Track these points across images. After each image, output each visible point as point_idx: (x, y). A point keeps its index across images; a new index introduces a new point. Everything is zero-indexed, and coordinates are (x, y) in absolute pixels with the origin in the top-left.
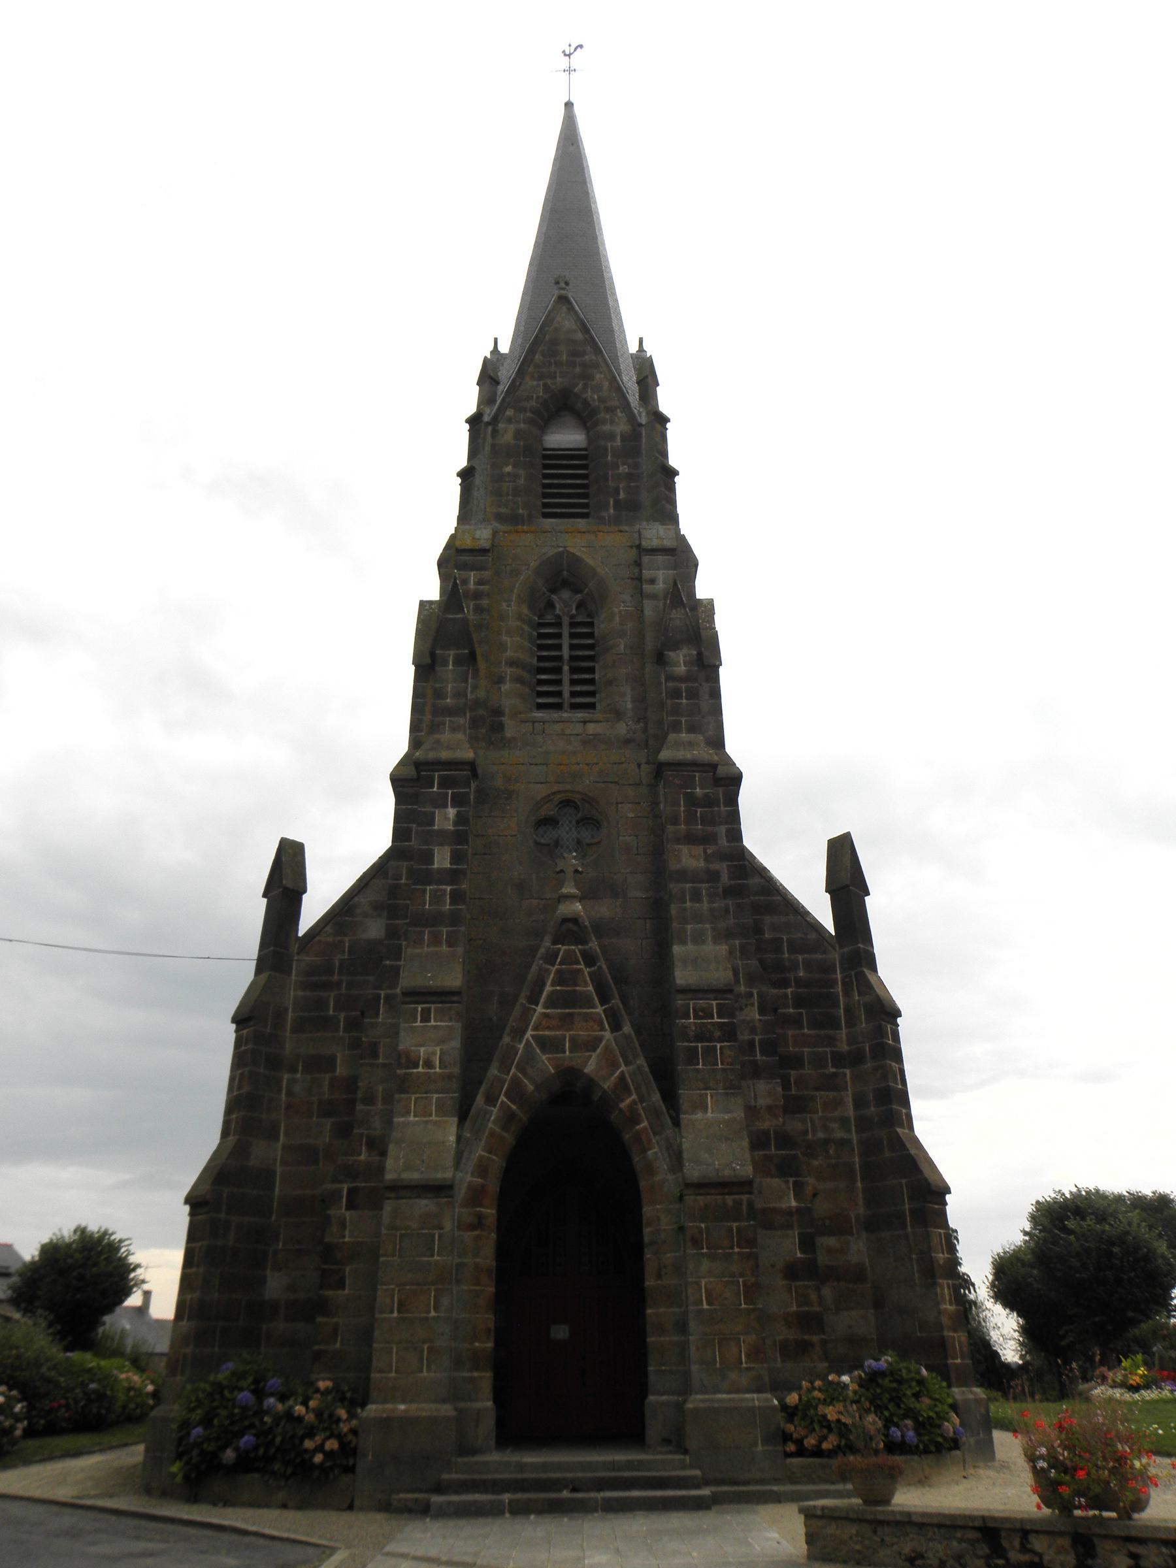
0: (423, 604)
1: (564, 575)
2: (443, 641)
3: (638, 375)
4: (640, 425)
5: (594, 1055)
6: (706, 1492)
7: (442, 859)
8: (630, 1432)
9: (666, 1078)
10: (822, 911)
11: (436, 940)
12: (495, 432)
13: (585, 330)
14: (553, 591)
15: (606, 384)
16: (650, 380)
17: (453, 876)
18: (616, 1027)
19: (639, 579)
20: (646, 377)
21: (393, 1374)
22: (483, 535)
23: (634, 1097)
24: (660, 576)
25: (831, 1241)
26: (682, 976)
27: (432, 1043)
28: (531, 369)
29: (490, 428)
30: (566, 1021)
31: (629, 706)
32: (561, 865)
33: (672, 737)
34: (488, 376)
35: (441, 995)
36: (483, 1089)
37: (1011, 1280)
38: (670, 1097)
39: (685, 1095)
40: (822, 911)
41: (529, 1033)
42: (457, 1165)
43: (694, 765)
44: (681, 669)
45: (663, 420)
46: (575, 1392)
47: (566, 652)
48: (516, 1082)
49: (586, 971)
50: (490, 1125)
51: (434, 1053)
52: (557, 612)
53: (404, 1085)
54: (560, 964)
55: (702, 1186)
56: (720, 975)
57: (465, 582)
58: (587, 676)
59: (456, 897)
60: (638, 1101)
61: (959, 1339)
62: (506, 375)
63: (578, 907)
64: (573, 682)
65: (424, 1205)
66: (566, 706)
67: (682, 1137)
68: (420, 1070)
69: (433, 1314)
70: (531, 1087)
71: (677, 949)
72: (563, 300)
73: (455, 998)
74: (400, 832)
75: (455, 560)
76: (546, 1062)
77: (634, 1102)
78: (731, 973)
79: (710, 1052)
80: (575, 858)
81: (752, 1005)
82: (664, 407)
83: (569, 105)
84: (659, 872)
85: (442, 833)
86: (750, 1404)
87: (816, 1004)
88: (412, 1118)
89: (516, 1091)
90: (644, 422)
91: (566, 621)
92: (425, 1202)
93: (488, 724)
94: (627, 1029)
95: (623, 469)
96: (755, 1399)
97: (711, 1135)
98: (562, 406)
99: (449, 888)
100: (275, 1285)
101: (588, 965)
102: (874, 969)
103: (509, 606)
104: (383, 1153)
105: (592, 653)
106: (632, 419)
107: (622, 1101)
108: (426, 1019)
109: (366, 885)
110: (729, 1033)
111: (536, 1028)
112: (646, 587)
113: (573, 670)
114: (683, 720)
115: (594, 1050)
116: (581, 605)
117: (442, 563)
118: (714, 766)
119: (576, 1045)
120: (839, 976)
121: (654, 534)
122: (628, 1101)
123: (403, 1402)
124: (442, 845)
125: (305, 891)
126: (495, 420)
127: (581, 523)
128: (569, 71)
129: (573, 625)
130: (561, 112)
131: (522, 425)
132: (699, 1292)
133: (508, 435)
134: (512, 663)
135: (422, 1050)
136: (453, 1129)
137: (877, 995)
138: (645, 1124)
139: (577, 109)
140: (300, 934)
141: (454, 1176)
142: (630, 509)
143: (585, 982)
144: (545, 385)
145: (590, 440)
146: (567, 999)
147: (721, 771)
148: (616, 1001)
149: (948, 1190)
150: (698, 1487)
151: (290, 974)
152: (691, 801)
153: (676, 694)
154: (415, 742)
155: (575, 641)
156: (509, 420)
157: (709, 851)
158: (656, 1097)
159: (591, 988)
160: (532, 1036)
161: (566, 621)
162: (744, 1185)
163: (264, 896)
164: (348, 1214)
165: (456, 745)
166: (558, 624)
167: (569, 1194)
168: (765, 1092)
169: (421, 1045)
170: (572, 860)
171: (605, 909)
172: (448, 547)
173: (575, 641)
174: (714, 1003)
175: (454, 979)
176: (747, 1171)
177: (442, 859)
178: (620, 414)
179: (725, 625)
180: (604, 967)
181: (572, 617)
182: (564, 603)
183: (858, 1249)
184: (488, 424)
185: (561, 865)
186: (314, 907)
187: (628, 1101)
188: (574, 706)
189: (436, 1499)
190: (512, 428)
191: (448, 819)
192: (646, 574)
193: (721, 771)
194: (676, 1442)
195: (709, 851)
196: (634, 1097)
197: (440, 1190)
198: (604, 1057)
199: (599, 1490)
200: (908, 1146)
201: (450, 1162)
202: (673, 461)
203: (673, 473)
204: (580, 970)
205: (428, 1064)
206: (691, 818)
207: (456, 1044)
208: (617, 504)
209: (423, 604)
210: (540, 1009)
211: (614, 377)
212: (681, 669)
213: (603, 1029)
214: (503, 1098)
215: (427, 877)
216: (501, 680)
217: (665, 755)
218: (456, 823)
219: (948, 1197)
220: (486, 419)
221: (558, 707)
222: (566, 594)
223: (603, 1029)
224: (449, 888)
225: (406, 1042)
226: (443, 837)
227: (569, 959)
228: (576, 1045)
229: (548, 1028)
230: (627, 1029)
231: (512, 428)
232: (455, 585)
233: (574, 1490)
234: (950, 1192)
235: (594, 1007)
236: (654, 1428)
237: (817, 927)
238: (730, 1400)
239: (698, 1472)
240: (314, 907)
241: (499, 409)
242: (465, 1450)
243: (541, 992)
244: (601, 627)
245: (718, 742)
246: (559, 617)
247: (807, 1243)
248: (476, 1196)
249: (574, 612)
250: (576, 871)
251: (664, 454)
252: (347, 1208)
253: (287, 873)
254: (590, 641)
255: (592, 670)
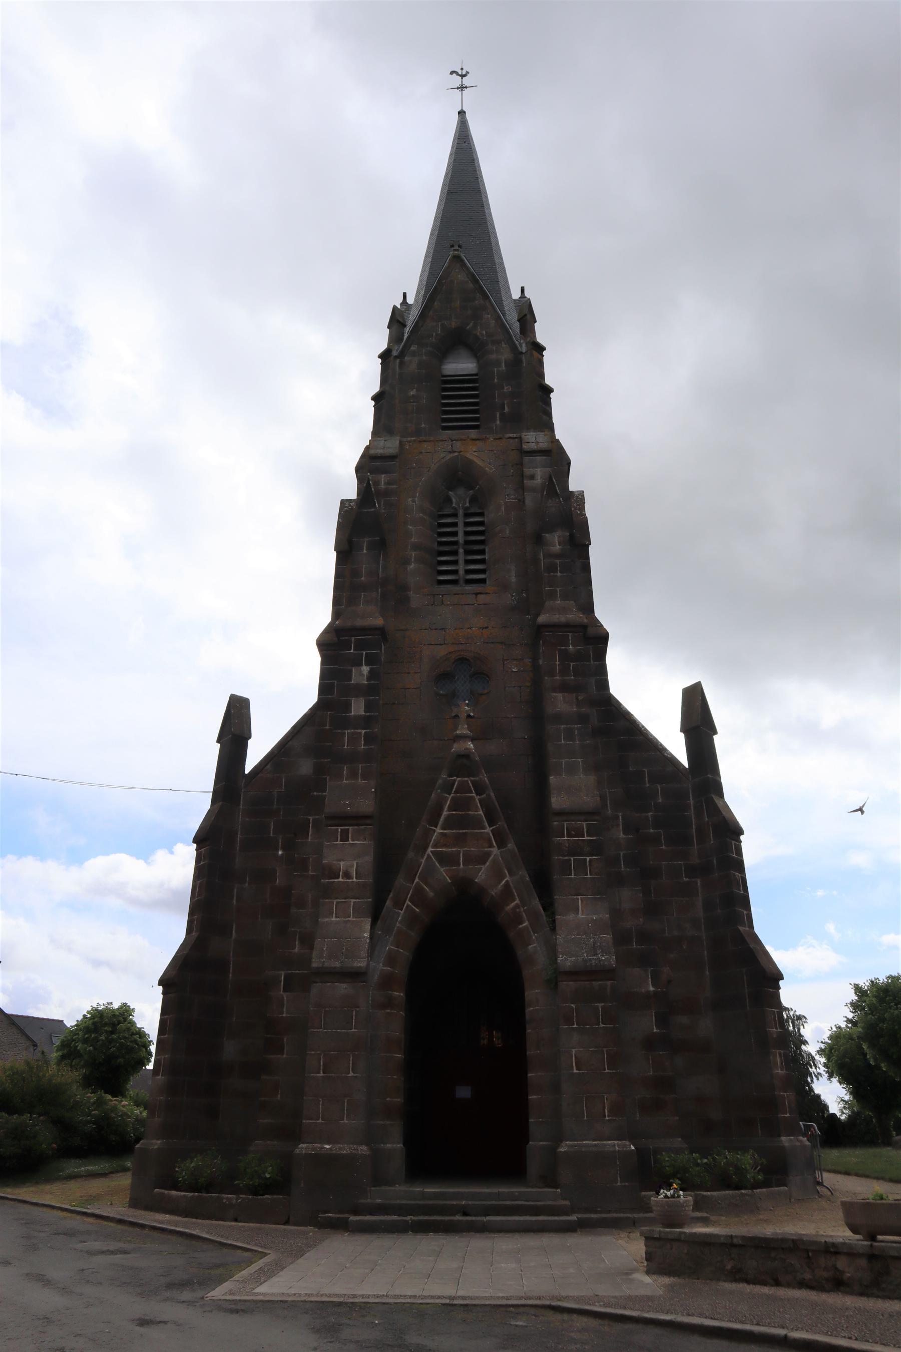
0: (343, 502)
1: (459, 475)
2: (362, 531)
3: (519, 314)
4: (522, 353)
5: (484, 868)
6: (573, 1218)
7: (358, 708)
8: (512, 1168)
9: (543, 886)
10: (676, 746)
11: (353, 774)
12: (402, 364)
13: (475, 281)
14: (451, 488)
15: (493, 322)
16: (528, 317)
17: (366, 722)
18: (501, 844)
19: (522, 475)
20: (525, 315)
21: (320, 1121)
22: (391, 445)
23: (517, 901)
24: (538, 473)
25: (684, 1020)
26: (557, 801)
27: (350, 858)
28: (431, 313)
29: (398, 361)
30: (460, 840)
31: (513, 579)
32: (455, 711)
33: (548, 604)
34: (397, 320)
35: (357, 819)
36: (391, 895)
37: (844, 1056)
38: (549, 906)
39: (559, 898)
40: (676, 746)
41: (430, 849)
42: (371, 954)
43: (567, 626)
44: (557, 548)
45: (540, 349)
46: (465, 1120)
47: (461, 538)
48: (419, 891)
49: (477, 798)
50: (398, 925)
51: (352, 866)
52: (454, 505)
53: (328, 892)
54: (456, 792)
55: (573, 974)
56: (588, 799)
57: (377, 483)
58: (479, 557)
59: (369, 739)
60: (521, 905)
61: (788, 1097)
62: (412, 317)
63: (471, 745)
64: (467, 562)
65: (343, 988)
66: (462, 582)
67: (557, 934)
68: (340, 879)
69: (351, 1074)
70: (431, 894)
71: (552, 779)
72: (457, 258)
73: (368, 821)
74: (325, 687)
75: (369, 466)
76: (444, 873)
77: (517, 906)
78: (598, 799)
79: (580, 865)
80: (468, 705)
81: (618, 825)
82: (540, 338)
83: (462, 113)
84: (537, 715)
85: (358, 687)
86: (611, 1149)
87: (676, 823)
88: (334, 919)
89: (419, 897)
90: (524, 351)
91: (461, 512)
92: (344, 986)
93: (395, 597)
94: (511, 845)
95: (507, 389)
96: (615, 1145)
97: (580, 930)
98: (457, 341)
99: (363, 731)
100: (230, 1050)
101: (477, 794)
102: (721, 794)
103: (413, 501)
104: (312, 948)
105: (483, 538)
106: (514, 348)
107: (508, 905)
108: (345, 838)
109: (298, 731)
110: (596, 848)
111: (435, 846)
112: (527, 482)
113: (467, 552)
114: (558, 589)
115: (484, 863)
116: (473, 500)
117: (359, 469)
118: (584, 627)
119: (468, 860)
120: (692, 802)
121: (533, 439)
122: (512, 905)
123: (328, 1143)
124: (357, 696)
125: (250, 737)
126: (402, 355)
127: (473, 433)
128: (462, 88)
129: (467, 515)
130: (456, 118)
131: (424, 358)
132: (567, 1053)
133: (412, 364)
134: (416, 547)
135: (342, 863)
136: (368, 927)
137: (724, 817)
138: (526, 924)
139: (468, 116)
140: (247, 772)
141: (368, 965)
142: (515, 420)
143: (477, 806)
144: (442, 325)
145: (481, 366)
146: (460, 822)
147: (591, 631)
148: (502, 823)
149: (780, 977)
150: (567, 1214)
151: (239, 805)
152: (565, 656)
153: (552, 568)
154: (337, 613)
155: (469, 529)
156: (414, 354)
157: (580, 698)
158: (536, 903)
159: (481, 812)
160: (432, 852)
161: (461, 512)
162: (605, 973)
163: (218, 741)
164: (285, 996)
165: (371, 616)
166: (455, 515)
167: (464, 1003)
168: (628, 897)
169: (340, 860)
170: (466, 708)
171: (493, 748)
172: (363, 456)
173: (469, 529)
174: (584, 824)
175: (366, 805)
176: (608, 959)
177: (358, 708)
178: (504, 345)
179: (591, 511)
180: (492, 794)
181: (466, 509)
182: (459, 498)
183: (706, 1026)
184: (396, 357)
185: (455, 711)
186: (256, 752)
187: (512, 905)
188: (469, 582)
189: (353, 1218)
190: (416, 360)
191: (363, 675)
192: (528, 471)
193: (591, 631)
194: (550, 1179)
195: (580, 698)
196: (517, 901)
197: (355, 976)
198: (495, 870)
199: (486, 1215)
200: (748, 941)
201: (364, 954)
202: (549, 381)
203: (549, 390)
204: (473, 797)
205: (347, 875)
206: (564, 671)
207: (369, 859)
208: (503, 415)
209: (343, 502)
210: (439, 830)
211: (499, 317)
212: (557, 548)
213: (491, 846)
214: (408, 902)
215: (345, 722)
216: (407, 562)
217: (542, 619)
218: (369, 679)
219: (781, 982)
220: (395, 353)
221: (455, 582)
222: (461, 491)
223: (491, 846)
224: (363, 731)
225: (329, 859)
226: (358, 691)
227: (463, 788)
228: (468, 860)
229: (445, 846)
230: (511, 845)
231: (416, 360)
232: (368, 484)
233: (465, 1214)
234: (782, 979)
235: (484, 828)
236: (534, 1166)
237: (673, 761)
238: (596, 1145)
239: (567, 1203)
240: (256, 752)
241: (404, 346)
242: (379, 1180)
243: (440, 815)
244: (490, 516)
245: (589, 608)
246: (454, 508)
247: (663, 1020)
248: (387, 982)
249: (467, 505)
250: (469, 716)
251: (542, 376)
252: (284, 991)
253: (236, 723)
254: (481, 528)
255: (482, 552)
